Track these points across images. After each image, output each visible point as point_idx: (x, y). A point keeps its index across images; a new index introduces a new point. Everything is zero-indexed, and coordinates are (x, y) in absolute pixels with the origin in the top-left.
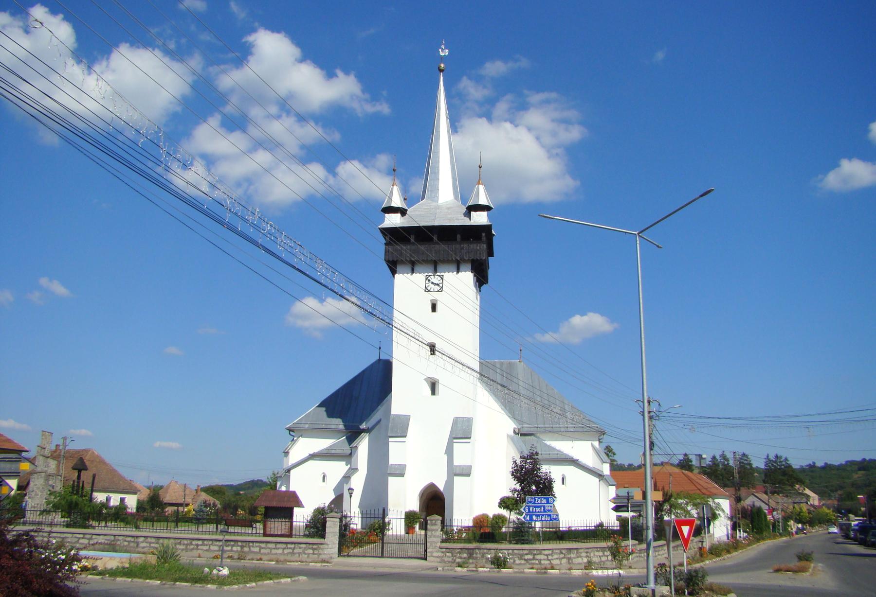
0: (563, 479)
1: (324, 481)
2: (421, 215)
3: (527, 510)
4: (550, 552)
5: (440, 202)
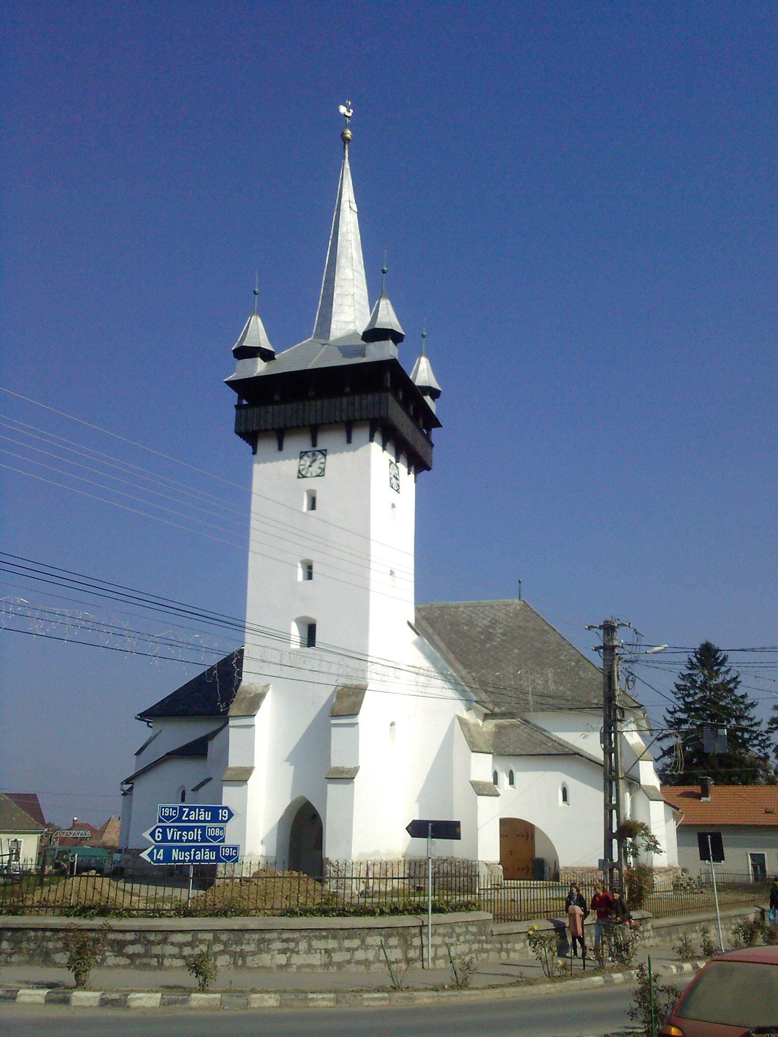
0: (565, 791)
1: (565, 798)
2: (296, 358)
3: (158, 836)
4: (188, 938)
5: (331, 338)
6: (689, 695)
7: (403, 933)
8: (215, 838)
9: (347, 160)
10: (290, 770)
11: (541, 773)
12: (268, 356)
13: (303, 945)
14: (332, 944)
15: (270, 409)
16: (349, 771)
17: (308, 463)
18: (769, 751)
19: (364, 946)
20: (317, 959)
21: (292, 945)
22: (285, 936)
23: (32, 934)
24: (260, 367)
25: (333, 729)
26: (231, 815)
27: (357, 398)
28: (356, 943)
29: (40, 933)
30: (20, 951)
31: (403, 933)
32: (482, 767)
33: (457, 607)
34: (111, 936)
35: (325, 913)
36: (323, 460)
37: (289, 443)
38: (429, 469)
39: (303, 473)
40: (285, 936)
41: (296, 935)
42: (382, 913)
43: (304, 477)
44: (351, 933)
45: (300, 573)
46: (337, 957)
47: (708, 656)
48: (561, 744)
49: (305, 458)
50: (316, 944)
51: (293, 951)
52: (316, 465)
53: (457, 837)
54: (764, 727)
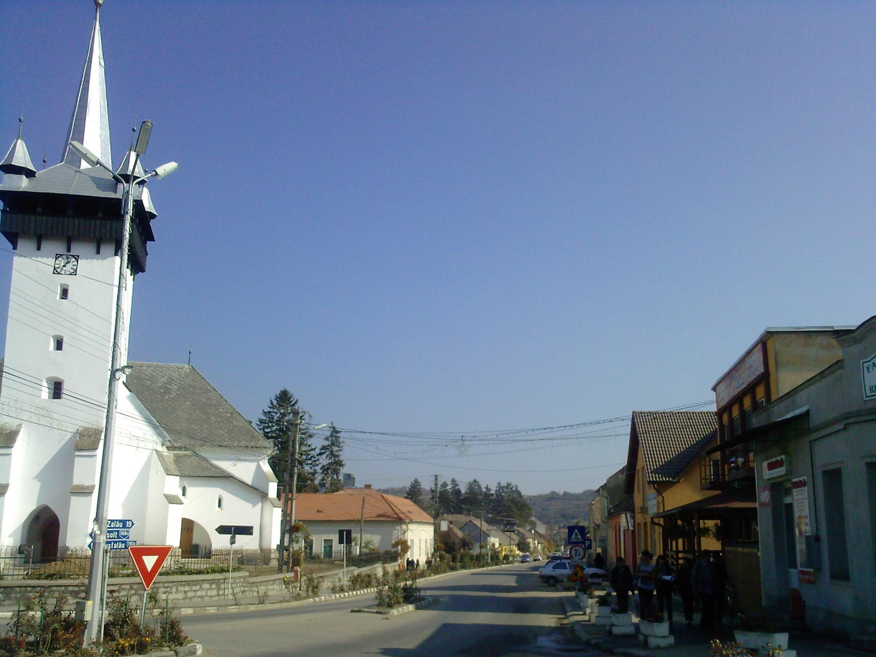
0: (220, 501)
1: (219, 506)
2: (53, 180)
6: (268, 427)
7: (217, 582)
8: (124, 536)
9: (98, 23)
10: (37, 485)
11: (206, 488)
12: (30, 174)
13: (174, 589)
14: (187, 588)
15: (33, 218)
16: (88, 488)
17: (63, 264)
18: (318, 468)
19: (201, 589)
20: (180, 596)
21: (169, 589)
22: (166, 585)
23: (18, 589)
24: (23, 184)
25: (76, 459)
26: (133, 524)
27: (108, 223)
28: (198, 587)
29: (23, 589)
30: (10, 598)
31: (217, 582)
32: (173, 485)
33: (141, 366)
34: (70, 588)
35: (182, 573)
36: (75, 263)
37: (45, 245)
38: (143, 271)
39: (59, 270)
40: (166, 585)
41: (171, 585)
42: (208, 573)
43: (59, 273)
44: (195, 583)
45: (52, 345)
46: (189, 595)
47: (284, 398)
48: (222, 471)
49: (60, 259)
50: (180, 588)
51: (169, 592)
52: (69, 266)
53: (251, 534)
54: (318, 451)
